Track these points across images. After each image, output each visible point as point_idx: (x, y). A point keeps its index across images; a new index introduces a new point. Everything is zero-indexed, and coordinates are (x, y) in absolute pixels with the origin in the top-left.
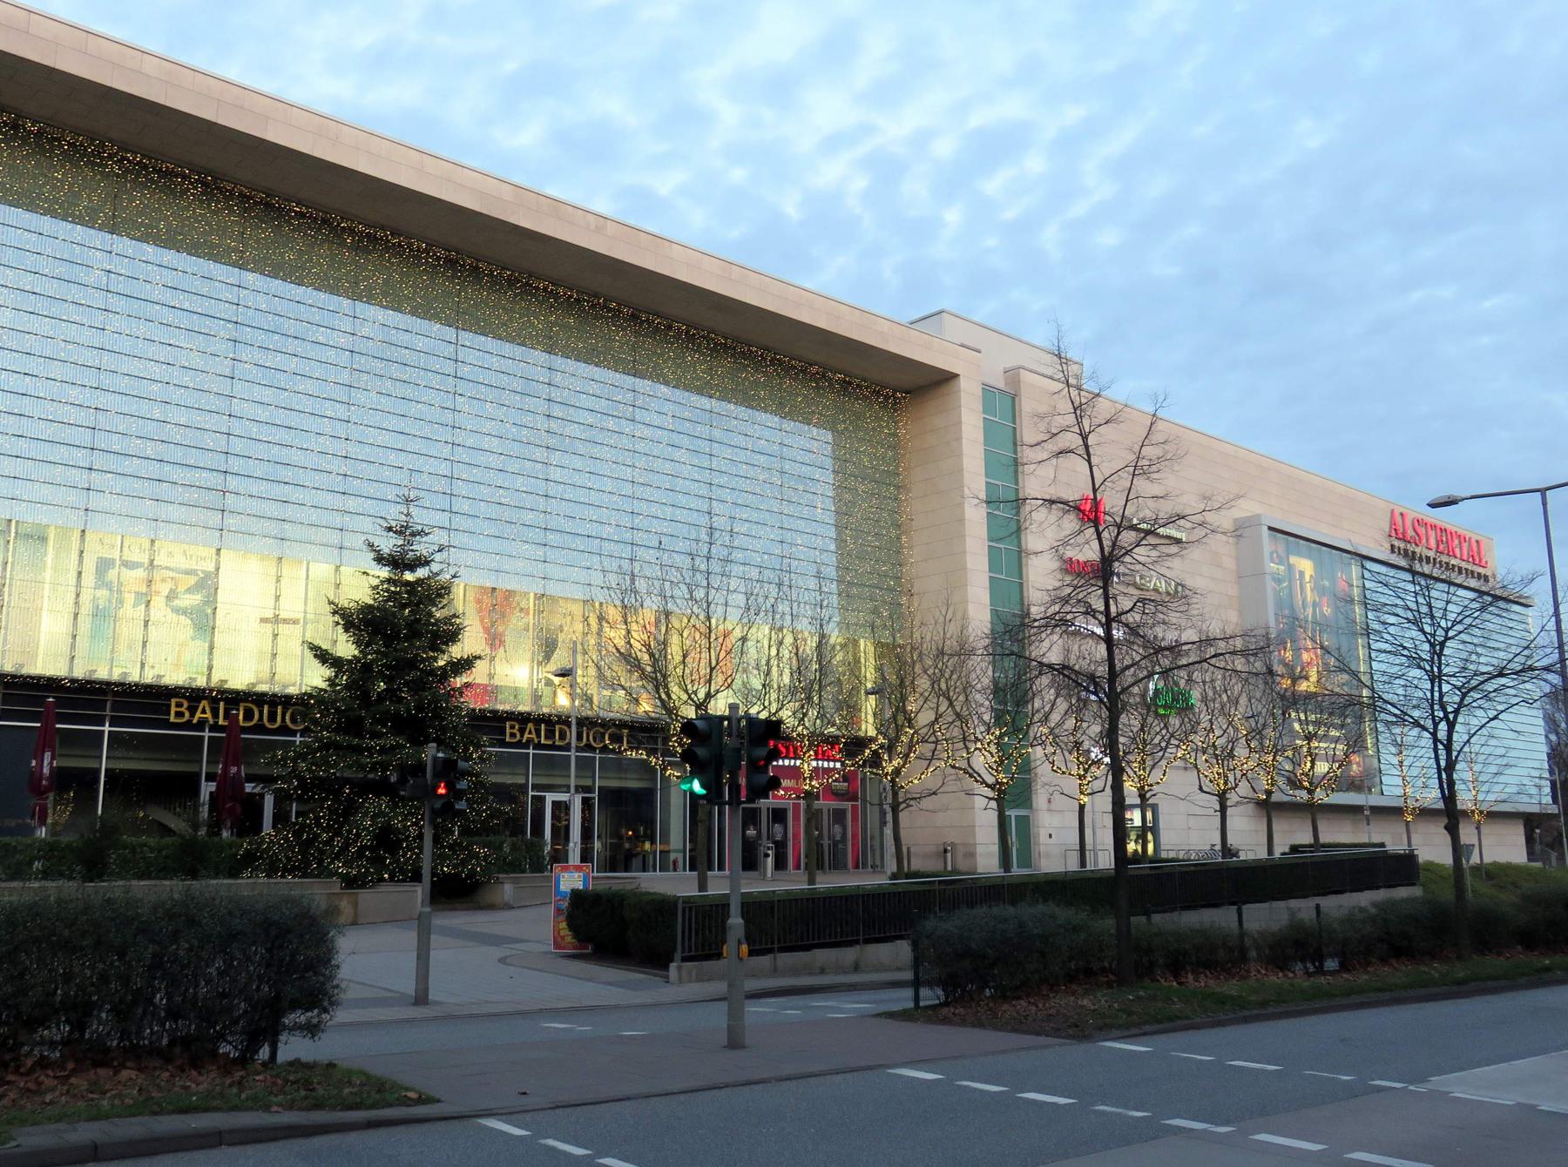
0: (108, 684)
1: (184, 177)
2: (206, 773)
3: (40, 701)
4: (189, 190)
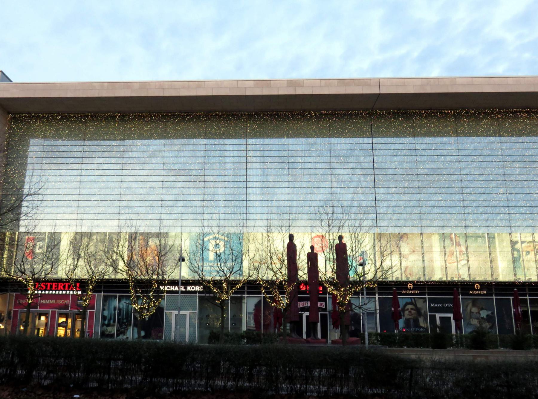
0: (525, 282)
1: (520, 112)
2: (531, 311)
3: (452, 289)
4: (522, 115)
